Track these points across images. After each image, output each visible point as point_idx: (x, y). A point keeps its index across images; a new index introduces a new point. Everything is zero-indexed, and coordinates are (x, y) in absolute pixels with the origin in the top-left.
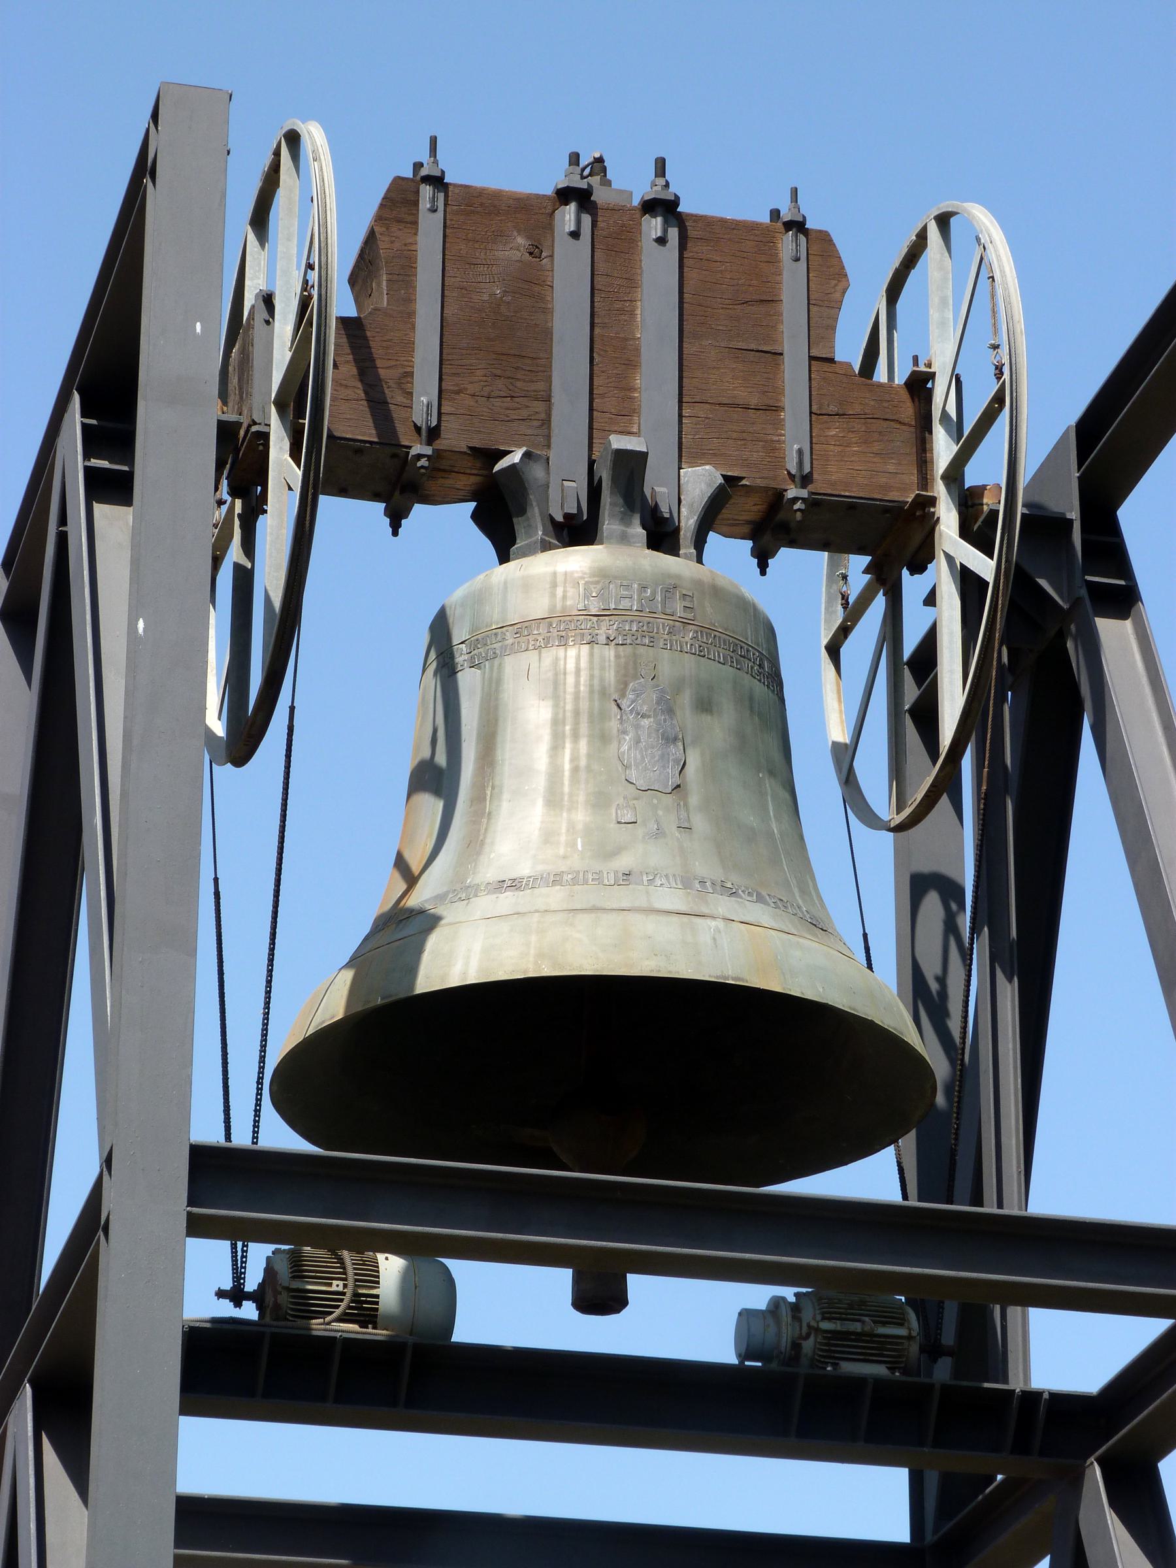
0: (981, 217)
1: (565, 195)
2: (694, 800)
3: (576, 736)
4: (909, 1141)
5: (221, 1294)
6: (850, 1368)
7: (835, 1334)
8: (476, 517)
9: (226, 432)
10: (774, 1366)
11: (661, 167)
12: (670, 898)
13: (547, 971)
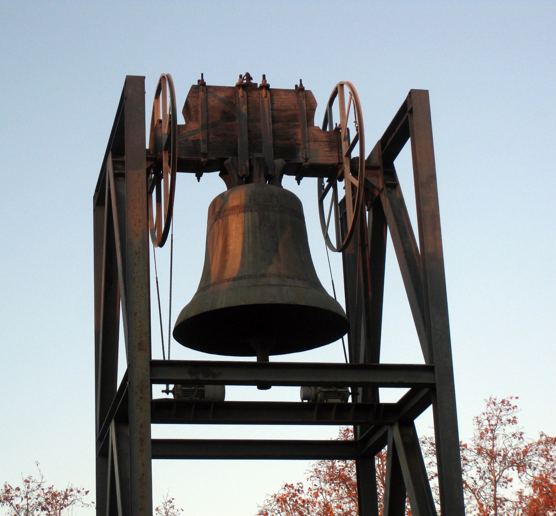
5: (163, 391)
6: (331, 401)
7: (327, 392)
8: (220, 175)
10: (310, 401)
13: (243, 303)
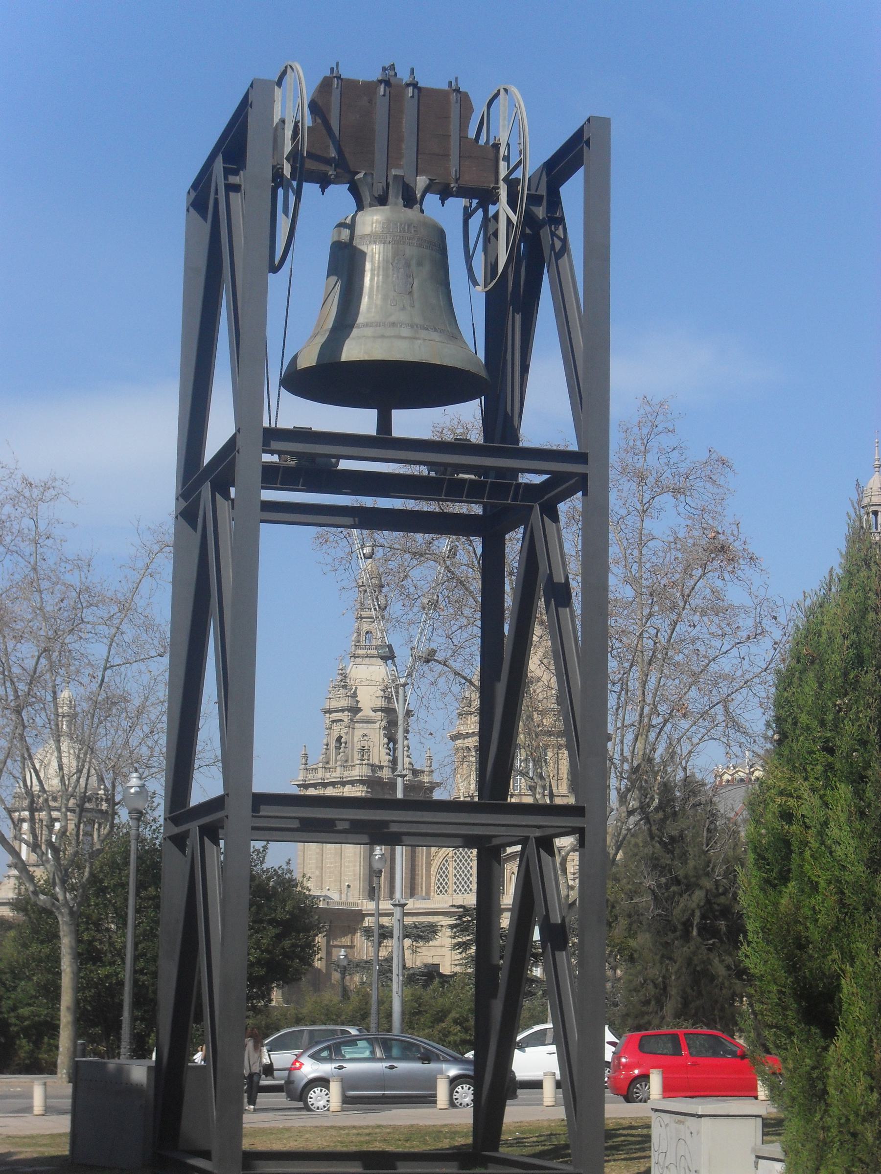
0: (514, 89)
1: (380, 82)
2: (416, 295)
3: (378, 276)
4: (483, 373)
11: (412, 71)
12: (406, 332)
13: (367, 358)
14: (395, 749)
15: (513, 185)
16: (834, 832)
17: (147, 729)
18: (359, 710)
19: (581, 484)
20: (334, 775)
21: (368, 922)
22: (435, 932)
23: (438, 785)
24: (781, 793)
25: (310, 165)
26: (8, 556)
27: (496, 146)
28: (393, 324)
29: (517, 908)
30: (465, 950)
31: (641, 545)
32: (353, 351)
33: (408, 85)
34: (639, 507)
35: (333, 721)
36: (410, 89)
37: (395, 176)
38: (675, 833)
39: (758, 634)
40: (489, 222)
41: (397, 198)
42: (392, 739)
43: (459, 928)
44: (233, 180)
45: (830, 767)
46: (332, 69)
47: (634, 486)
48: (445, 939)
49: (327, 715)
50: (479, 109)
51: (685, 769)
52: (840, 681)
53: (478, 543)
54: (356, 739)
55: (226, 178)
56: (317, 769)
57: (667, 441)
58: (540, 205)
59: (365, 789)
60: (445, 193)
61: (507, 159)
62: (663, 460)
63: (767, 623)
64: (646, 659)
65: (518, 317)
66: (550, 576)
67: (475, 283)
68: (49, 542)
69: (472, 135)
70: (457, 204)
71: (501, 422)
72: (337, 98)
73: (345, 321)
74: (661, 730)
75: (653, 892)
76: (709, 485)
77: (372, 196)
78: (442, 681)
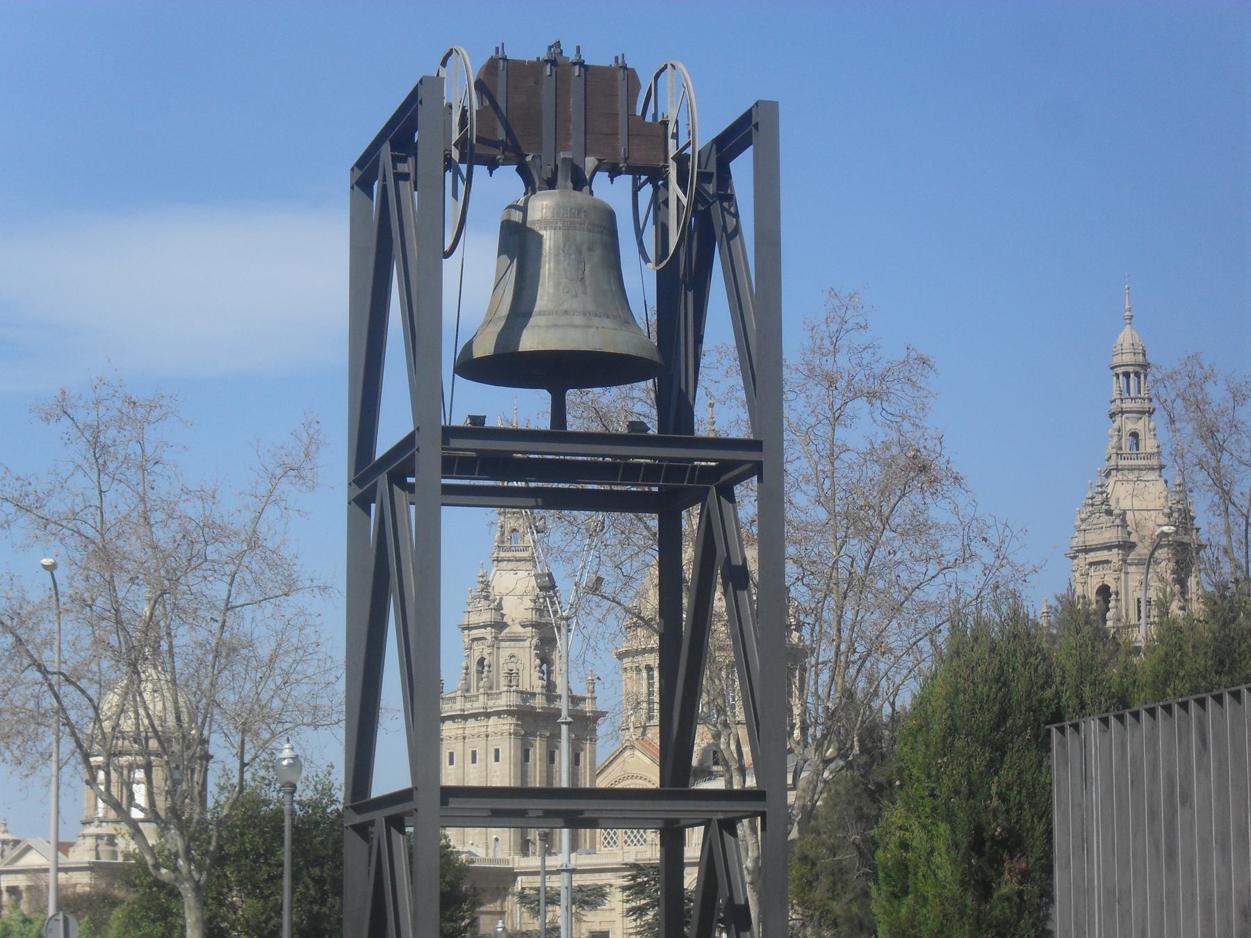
0: (680, 66)
1: (546, 61)
2: (587, 282)
4: (656, 357)
9: (445, 156)
12: (578, 320)
13: (541, 348)
14: (549, 672)
15: (681, 159)
16: (937, 859)
17: (279, 680)
18: (505, 625)
19: (757, 469)
20: (476, 705)
21: (521, 882)
22: (604, 896)
23: (603, 714)
24: (901, 828)
25: (480, 150)
26: (114, 486)
27: (665, 124)
28: (566, 312)
29: (704, 862)
30: (641, 916)
31: (832, 457)
32: (529, 341)
33: (575, 64)
34: (830, 415)
35: (474, 640)
36: (577, 68)
37: (564, 160)
38: (881, 779)
39: (967, 556)
40: (659, 204)
41: (566, 179)
42: (545, 660)
43: (636, 890)
44: (402, 168)
45: (934, 809)
46: (497, 49)
47: (824, 391)
48: (616, 902)
49: (466, 632)
50: (646, 81)
51: (893, 704)
52: (940, 746)
53: (653, 521)
54: (502, 661)
55: (395, 167)
56: (455, 698)
57: (859, 339)
58: (710, 182)
59: (514, 721)
60: (614, 172)
61: (676, 136)
62: (855, 361)
63: (977, 547)
64: (842, 591)
65: (690, 295)
66: (728, 559)
67: (647, 260)
68: (158, 468)
69: (639, 113)
70: (625, 181)
71: (676, 406)
72: (499, 77)
73: (520, 312)
74: (862, 666)
75: (858, 847)
76: (908, 388)
77: (541, 179)
78: (611, 619)
